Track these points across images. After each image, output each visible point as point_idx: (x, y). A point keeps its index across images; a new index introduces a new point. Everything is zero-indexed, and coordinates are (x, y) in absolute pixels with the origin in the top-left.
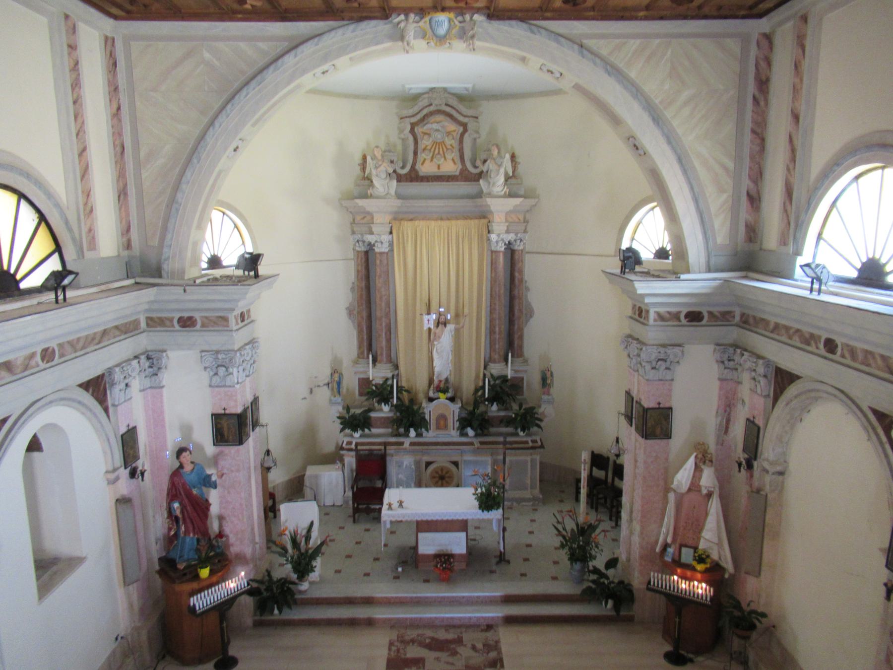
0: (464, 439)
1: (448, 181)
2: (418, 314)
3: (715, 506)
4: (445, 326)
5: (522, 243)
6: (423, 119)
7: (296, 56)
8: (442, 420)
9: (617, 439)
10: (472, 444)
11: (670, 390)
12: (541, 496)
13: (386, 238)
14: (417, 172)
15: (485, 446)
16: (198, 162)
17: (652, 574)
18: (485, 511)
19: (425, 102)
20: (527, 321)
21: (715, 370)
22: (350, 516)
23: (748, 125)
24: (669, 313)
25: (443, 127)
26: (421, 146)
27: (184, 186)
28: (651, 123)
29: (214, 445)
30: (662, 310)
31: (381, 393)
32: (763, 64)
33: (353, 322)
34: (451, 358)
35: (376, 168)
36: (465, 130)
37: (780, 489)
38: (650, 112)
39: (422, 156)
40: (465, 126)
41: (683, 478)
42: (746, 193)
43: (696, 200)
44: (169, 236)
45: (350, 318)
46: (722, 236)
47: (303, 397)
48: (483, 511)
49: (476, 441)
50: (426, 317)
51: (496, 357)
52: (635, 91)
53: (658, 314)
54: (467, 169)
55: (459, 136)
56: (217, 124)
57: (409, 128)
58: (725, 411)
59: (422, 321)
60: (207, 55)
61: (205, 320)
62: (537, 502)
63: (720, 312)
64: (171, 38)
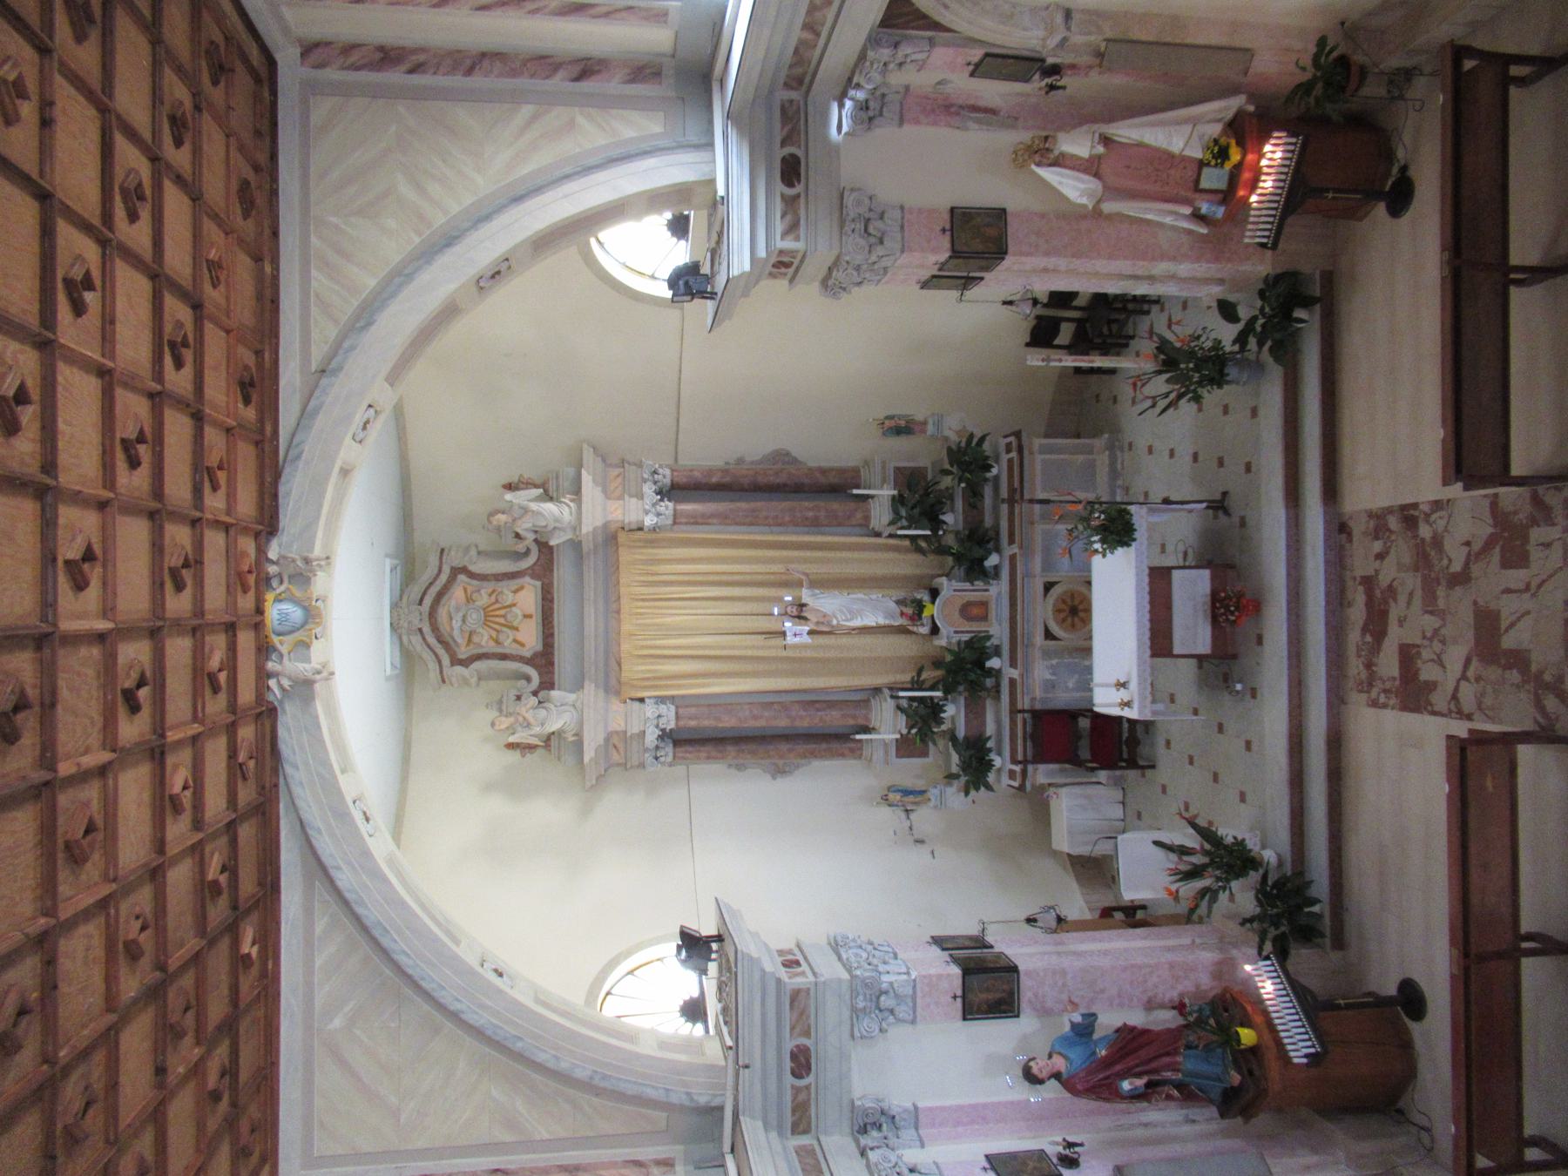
1: (552, 601)
2: (784, 654)
3: (1127, 131)
5: (661, 471)
6: (441, 641)
7: (338, 868)
8: (966, 611)
9: (1005, 303)
10: (1013, 558)
11: (920, 211)
12: (1106, 436)
13: (650, 710)
14: (536, 655)
15: (1017, 538)
16: (520, 1039)
19: (416, 640)
20: (795, 461)
23: (457, 81)
24: (783, 217)
25: (458, 609)
26: (492, 648)
27: (564, 1065)
28: (457, 249)
29: (1018, 1016)
30: (779, 227)
31: (924, 718)
32: (354, 58)
33: (798, 767)
34: (860, 596)
35: (528, 725)
36: (464, 570)
37: (1096, 15)
38: (436, 253)
39: (508, 646)
40: (456, 571)
41: (1074, 188)
42: (577, 84)
43: (588, 170)
44: (651, 1093)
45: (790, 772)
46: (651, 125)
47: (930, 856)
48: (1134, 540)
49: (1008, 551)
50: (790, 639)
52: (400, 277)
53: (785, 234)
54: (532, 568)
55: (475, 582)
56: (455, 1006)
57: (459, 669)
58: (958, 114)
59: (795, 647)
60: (337, 1022)
61: (797, 1030)
63: (782, 128)
64: (308, 1083)
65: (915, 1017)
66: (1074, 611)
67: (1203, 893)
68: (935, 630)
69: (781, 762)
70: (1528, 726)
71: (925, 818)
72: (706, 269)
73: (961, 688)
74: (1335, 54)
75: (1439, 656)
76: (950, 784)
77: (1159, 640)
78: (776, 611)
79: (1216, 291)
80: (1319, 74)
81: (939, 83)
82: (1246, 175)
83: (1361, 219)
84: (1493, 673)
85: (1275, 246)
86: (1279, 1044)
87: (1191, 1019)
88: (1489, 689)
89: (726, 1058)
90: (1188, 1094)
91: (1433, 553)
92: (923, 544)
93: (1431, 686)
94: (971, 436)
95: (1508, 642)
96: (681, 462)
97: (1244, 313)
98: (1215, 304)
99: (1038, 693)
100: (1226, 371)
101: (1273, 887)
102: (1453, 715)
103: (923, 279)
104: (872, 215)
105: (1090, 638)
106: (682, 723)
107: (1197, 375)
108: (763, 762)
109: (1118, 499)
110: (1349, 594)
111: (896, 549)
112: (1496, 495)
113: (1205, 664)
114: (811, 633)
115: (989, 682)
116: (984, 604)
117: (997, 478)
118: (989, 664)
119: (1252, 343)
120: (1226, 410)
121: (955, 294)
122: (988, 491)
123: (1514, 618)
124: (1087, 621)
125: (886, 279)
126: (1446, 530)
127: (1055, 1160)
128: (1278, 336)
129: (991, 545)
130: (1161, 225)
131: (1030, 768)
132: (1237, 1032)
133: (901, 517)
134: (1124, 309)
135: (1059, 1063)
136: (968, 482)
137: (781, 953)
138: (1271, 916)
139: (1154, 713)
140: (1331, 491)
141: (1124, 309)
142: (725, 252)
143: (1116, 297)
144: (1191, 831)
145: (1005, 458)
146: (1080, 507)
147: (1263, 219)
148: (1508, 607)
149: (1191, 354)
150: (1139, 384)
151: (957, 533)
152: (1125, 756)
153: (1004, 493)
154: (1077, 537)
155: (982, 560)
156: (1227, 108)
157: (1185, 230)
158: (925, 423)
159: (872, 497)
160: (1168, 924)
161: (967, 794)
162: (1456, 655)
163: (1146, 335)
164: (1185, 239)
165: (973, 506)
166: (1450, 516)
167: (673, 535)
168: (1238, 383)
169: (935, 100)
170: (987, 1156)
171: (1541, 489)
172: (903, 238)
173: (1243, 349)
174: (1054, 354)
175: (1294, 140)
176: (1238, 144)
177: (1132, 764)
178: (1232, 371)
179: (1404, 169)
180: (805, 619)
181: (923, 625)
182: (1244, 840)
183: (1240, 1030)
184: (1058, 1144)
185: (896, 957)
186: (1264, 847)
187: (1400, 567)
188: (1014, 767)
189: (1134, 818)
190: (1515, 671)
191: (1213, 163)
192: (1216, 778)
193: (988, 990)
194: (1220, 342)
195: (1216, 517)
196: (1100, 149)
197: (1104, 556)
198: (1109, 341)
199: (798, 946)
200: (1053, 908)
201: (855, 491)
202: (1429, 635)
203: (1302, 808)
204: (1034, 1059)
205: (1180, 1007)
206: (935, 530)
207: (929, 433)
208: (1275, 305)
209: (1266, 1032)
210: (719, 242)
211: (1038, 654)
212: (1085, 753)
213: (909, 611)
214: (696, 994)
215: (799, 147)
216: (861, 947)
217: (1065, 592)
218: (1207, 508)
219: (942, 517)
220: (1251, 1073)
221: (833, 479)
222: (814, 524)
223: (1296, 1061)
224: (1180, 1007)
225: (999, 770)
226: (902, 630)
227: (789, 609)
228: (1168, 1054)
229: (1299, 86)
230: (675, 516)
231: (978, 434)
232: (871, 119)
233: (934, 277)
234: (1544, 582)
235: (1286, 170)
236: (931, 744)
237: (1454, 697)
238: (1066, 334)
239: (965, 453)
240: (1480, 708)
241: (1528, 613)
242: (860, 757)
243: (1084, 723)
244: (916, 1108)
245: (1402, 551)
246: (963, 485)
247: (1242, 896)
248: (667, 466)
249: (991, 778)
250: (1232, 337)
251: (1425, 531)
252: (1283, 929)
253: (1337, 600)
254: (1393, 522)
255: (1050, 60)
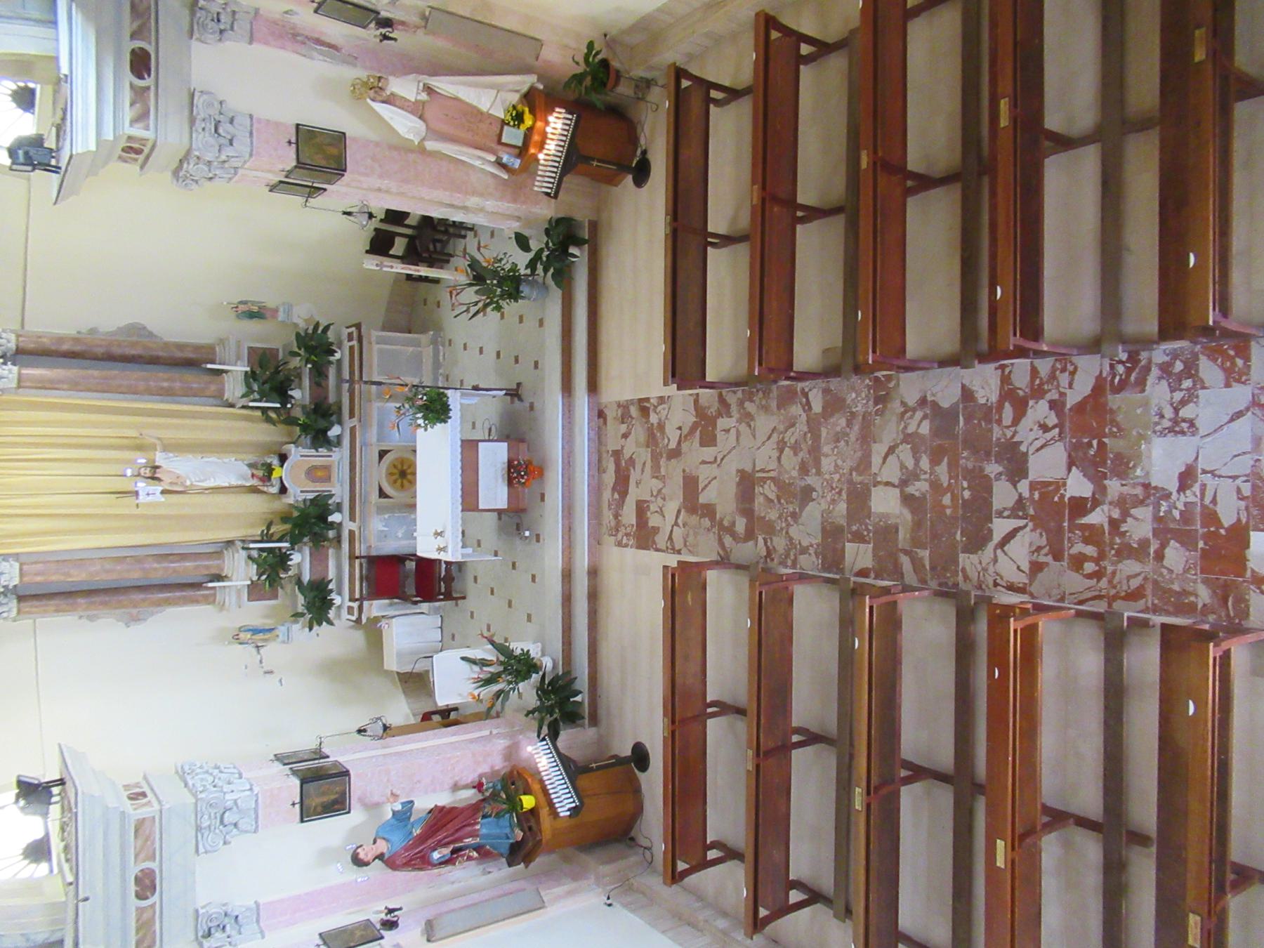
0: (346, 442)
3: (445, 85)
4: (158, 467)
8: (311, 473)
9: (345, 213)
10: (353, 430)
17: (536, 189)
18: (450, 415)
20: (151, 334)
21: (235, 48)
22: (457, 605)
24: (132, 105)
29: (349, 812)
30: (128, 114)
33: (152, 614)
41: (406, 126)
45: (145, 620)
48: (450, 418)
50: (142, 498)
51: (213, 388)
53: (134, 121)
58: (304, 43)
59: (149, 505)
61: (142, 856)
62: (439, 339)
63: (132, 23)
65: (257, 827)
66: (403, 474)
67: (498, 694)
68: (283, 490)
69: (134, 611)
70: (714, 557)
71: (274, 652)
72: (50, 143)
73: (306, 539)
74: (600, 57)
75: (661, 509)
76: (296, 622)
77: (469, 498)
78: (129, 472)
79: (516, 226)
80: (588, 70)
81: (286, 12)
82: (536, 138)
83: (616, 186)
84: (694, 519)
85: (556, 197)
86: (551, 804)
87: (487, 794)
88: (691, 533)
89: (66, 894)
90: (484, 853)
91: (659, 435)
92: (273, 415)
93: (656, 530)
94: (317, 325)
95: (703, 499)
96: (27, 328)
97: (535, 245)
98: (513, 236)
99: (374, 542)
100: (521, 289)
101: (549, 684)
102: (669, 551)
103: (272, 183)
104: (222, 118)
105: (415, 497)
106: (26, 579)
107: (499, 290)
108: (117, 611)
109: (440, 385)
110: (604, 463)
111: (246, 418)
112: (698, 394)
113: (503, 516)
114: (163, 492)
115: (331, 534)
116: (327, 468)
117: (339, 362)
118: (330, 519)
119: (540, 268)
120: (521, 319)
121: (301, 200)
122: (332, 372)
123: (707, 482)
124: (413, 483)
125: (236, 178)
126: (667, 418)
127: (378, 926)
128: (557, 265)
129: (334, 418)
130: (472, 166)
131: (366, 603)
132: (520, 800)
133: (253, 392)
134: (446, 232)
135: (382, 847)
136: (314, 363)
137: (126, 787)
138: (547, 707)
139: (463, 555)
140: (593, 386)
141: (446, 232)
142: (68, 129)
143: (441, 220)
144: (490, 646)
145: (347, 345)
146: (406, 389)
147: (548, 174)
148: (704, 474)
149: (495, 273)
150: (455, 293)
151: (304, 407)
152: (443, 590)
153: (346, 376)
154: (404, 414)
155: (325, 431)
156: (524, 83)
157: (492, 173)
158: (276, 311)
159: (226, 372)
160: (474, 721)
161: (311, 629)
162: (672, 507)
163: (461, 254)
164: (491, 181)
165: (318, 385)
166: (669, 409)
167: (16, 398)
168: (529, 299)
169: (284, 26)
170: (320, 934)
171: (724, 392)
172: (252, 143)
173: (533, 273)
174: (387, 261)
175: (570, 117)
176: (531, 112)
177: (448, 596)
178: (525, 289)
179: (644, 152)
180: (159, 479)
181: (272, 486)
182: (528, 651)
183: (523, 798)
184: (381, 912)
185: (241, 777)
186: (543, 655)
187: (638, 444)
188: (351, 604)
189: (448, 640)
190: (707, 519)
191: (512, 123)
192: (510, 605)
193: (324, 794)
194: (516, 265)
195: (512, 402)
196: (424, 96)
197: (426, 430)
198: (434, 256)
199: (145, 778)
200: (379, 718)
201: (209, 366)
202: (655, 493)
203: (570, 624)
204: (361, 846)
205: (479, 786)
206: (284, 405)
207: (280, 319)
208: (556, 241)
209: (541, 796)
210: (64, 119)
211: (374, 509)
212: (411, 589)
213: (260, 473)
214: (39, 834)
215: (150, 43)
216: (207, 772)
217: (397, 459)
218: (506, 394)
219: (290, 393)
220: (530, 828)
221: (189, 354)
222: (168, 394)
223: (562, 814)
224: (479, 786)
225: (339, 607)
226: (254, 490)
227: (142, 471)
228: (469, 825)
229: (575, 76)
230: (19, 380)
231: (324, 323)
232: (221, 32)
233: (281, 182)
234: (724, 456)
235: (564, 138)
236: (280, 590)
237: (670, 538)
238: (399, 246)
239: (312, 339)
240: (685, 545)
241: (715, 478)
242: (210, 600)
243: (411, 565)
244: (257, 904)
245: (639, 433)
246: (309, 366)
247: (527, 691)
248: (12, 331)
249: (332, 614)
250: (527, 262)
251: (654, 419)
252: (555, 716)
253: (597, 467)
254: (634, 411)
255: (384, 14)
